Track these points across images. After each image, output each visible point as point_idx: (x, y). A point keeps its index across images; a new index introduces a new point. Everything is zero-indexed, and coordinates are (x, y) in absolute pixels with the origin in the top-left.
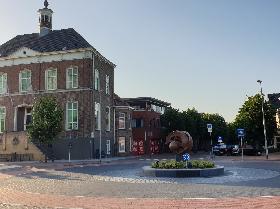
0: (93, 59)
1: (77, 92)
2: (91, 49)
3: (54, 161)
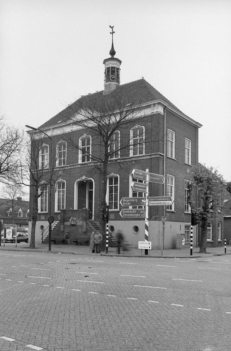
0: (164, 115)
1: (60, 136)
2: (160, 101)
3: (207, 249)
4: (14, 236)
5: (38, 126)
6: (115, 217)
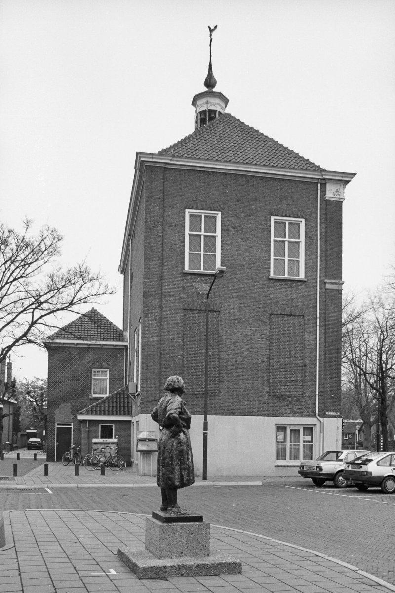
4: (308, 438)
5: (64, 235)
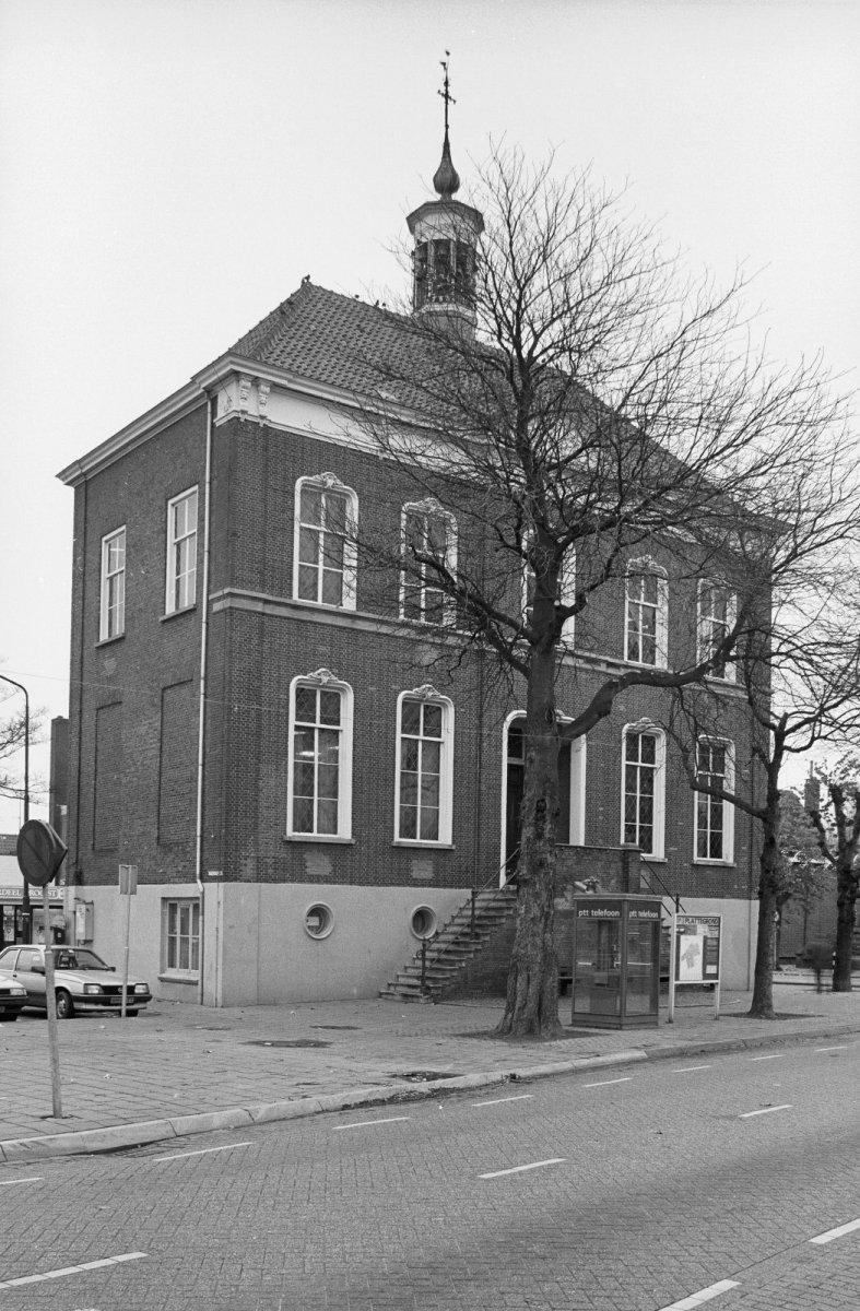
6: (436, 872)
